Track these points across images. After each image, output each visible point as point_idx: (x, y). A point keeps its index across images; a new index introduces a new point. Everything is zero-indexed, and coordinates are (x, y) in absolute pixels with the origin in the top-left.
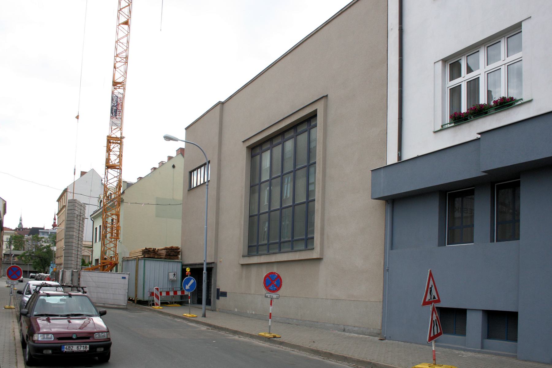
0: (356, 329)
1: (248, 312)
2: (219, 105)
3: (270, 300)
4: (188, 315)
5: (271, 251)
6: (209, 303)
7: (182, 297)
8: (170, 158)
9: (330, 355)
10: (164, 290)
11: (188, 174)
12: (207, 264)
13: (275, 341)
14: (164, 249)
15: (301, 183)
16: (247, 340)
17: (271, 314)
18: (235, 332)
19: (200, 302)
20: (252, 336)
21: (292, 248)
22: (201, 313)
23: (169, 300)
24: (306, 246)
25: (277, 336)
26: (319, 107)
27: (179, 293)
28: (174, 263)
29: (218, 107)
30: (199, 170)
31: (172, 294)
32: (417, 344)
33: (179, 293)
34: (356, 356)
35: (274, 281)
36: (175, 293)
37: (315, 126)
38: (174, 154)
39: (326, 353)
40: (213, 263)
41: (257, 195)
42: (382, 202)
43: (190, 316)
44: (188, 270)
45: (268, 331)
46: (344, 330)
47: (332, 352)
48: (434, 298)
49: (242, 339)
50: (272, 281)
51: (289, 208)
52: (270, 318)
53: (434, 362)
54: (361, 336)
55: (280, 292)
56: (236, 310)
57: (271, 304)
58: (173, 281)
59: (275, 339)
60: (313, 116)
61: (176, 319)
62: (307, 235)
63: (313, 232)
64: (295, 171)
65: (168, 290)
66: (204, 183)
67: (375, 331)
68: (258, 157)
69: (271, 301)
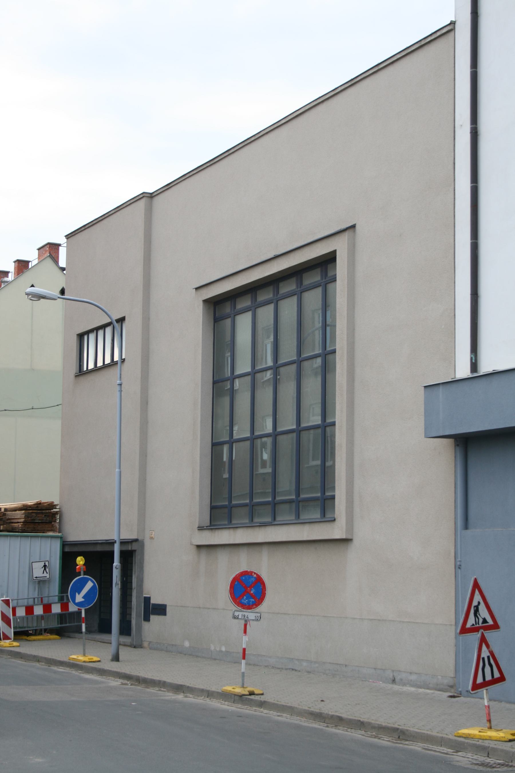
0: (413, 677)
1: (212, 648)
2: (143, 201)
3: (243, 622)
4: (82, 658)
5: (256, 520)
6: (125, 629)
7: (61, 617)
8: (22, 266)
9: (339, 721)
10: (21, 602)
11: (74, 340)
12: (123, 543)
13: (252, 700)
14: (20, 509)
15: (312, 386)
16: (200, 700)
17: (244, 650)
18: (178, 688)
19: (105, 627)
20: (210, 694)
21: (298, 516)
22: (109, 651)
23: (33, 625)
24: (324, 514)
25: (256, 692)
26: (340, 246)
27: (56, 609)
28: (44, 540)
29: (142, 203)
30: (101, 333)
31: (38, 610)
32: (510, 702)
33: (56, 609)
34: (382, 721)
35: (251, 587)
36: (47, 608)
37: (334, 280)
38: (32, 256)
39: (332, 716)
40: (136, 540)
41: (226, 400)
42: (450, 441)
43: (86, 659)
44: (80, 561)
45: (241, 684)
46: (394, 681)
47: (344, 716)
48: (485, 621)
49: (191, 699)
50: (246, 587)
51: (290, 435)
52: (244, 658)
53: (488, 725)
54: (421, 690)
55: (263, 607)
56: (187, 644)
57: (245, 632)
58: (41, 582)
59: (252, 697)
60: (330, 259)
61: (55, 668)
62: (324, 491)
63: (333, 488)
64: (299, 362)
65: (31, 602)
66: (113, 363)
67: (446, 681)
68: (228, 322)
69: (245, 626)
